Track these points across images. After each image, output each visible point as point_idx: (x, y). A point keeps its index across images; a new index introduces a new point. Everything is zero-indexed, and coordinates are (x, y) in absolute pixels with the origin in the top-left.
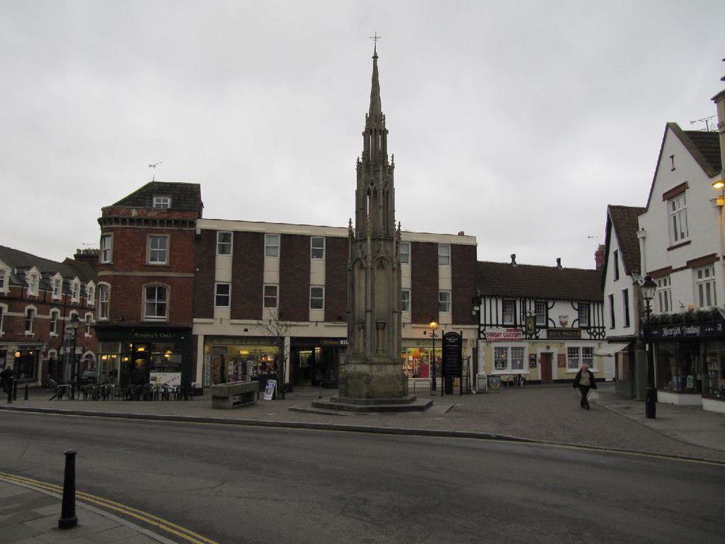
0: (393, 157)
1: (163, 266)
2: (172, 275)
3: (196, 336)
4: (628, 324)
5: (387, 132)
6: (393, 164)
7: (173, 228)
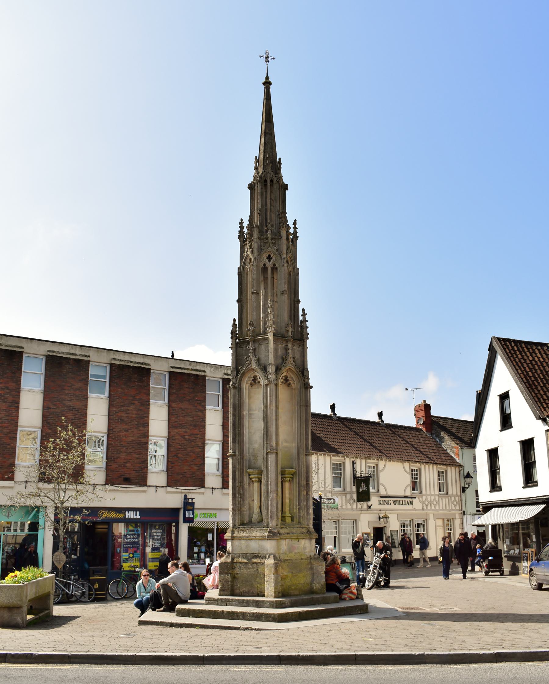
0: (295, 223)
4: (493, 454)
5: (285, 187)
6: (295, 233)
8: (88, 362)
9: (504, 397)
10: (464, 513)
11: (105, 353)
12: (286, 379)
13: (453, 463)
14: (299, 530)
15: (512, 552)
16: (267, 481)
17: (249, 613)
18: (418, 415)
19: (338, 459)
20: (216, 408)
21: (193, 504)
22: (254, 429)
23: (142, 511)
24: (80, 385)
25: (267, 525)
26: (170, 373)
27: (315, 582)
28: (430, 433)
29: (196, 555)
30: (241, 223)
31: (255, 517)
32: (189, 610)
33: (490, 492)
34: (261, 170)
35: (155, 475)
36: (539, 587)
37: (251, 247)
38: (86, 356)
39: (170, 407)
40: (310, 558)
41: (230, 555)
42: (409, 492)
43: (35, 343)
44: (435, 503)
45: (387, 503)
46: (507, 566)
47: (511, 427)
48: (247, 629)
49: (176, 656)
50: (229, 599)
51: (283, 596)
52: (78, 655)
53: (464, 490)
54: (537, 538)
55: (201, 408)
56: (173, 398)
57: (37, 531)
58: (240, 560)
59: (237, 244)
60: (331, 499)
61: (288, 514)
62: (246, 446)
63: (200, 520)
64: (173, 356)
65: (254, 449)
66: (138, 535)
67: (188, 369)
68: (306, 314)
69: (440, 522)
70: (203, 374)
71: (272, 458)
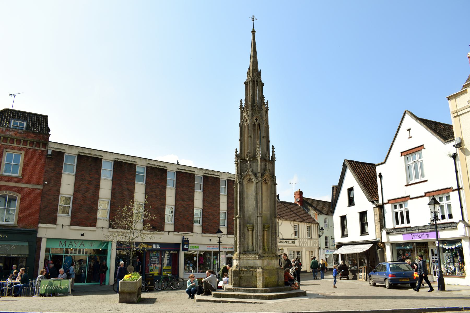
1: (15, 177)
2: (24, 185)
3: (40, 239)
4: (343, 218)
5: (263, 84)
7: (28, 147)
8: (136, 164)
9: (351, 190)
11: (144, 161)
12: (265, 180)
13: (315, 222)
14: (272, 255)
15: (353, 268)
16: (257, 230)
20: (199, 191)
21: (188, 241)
22: (250, 204)
23: (161, 244)
24: (131, 177)
26: (177, 172)
29: (187, 268)
30: (241, 101)
31: (250, 248)
32: (220, 294)
34: (251, 75)
35: (168, 225)
36: (374, 285)
37: (247, 113)
38: (134, 162)
39: (176, 190)
40: (277, 269)
42: (293, 237)
43: (108, 154)
45: (283, 242)
46: (351, 276)
47: (354, 205)
48: (255, 303)
51: (265, 288)
53: (319, 236)
54: (368, 261)
55: (192, 191)
56: (178, 185)
57: (211, 252)
58: (243, 269)
59: (239, 111)
61: (266, 247)
62: (246, 213)
63: (191, 250)
64: (178, 163)
66: (158, 257)
67: (186, 170)
69: (308, 253)
70: (193, 173)
71: (259, 219)
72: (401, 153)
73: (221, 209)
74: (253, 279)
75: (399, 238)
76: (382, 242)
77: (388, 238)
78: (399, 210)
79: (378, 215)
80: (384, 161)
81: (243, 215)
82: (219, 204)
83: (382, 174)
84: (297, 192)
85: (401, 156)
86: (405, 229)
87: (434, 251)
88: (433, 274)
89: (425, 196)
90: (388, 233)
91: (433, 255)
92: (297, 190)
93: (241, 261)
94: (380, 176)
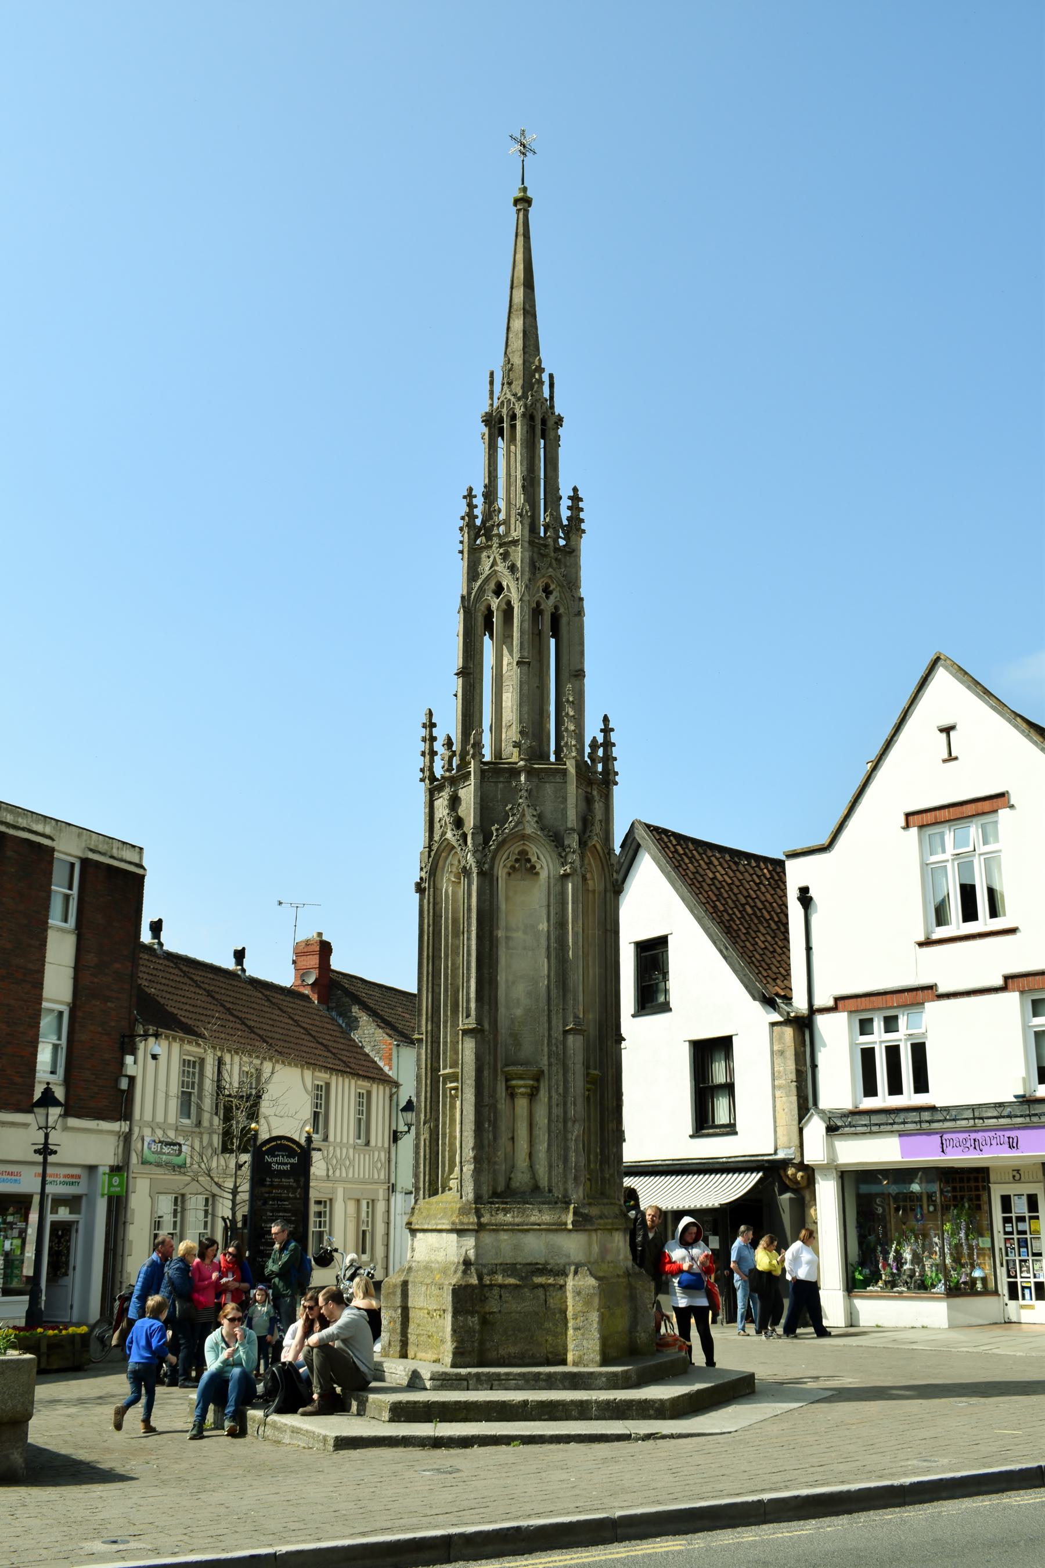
10: (392, 1189)
17: (596, 1402)
18: (300, 964)
19: (194, 1050)
25: (565, 1196)
27: (639, 1328)
28: (325, 1007)
33: (691, 1136)
40: (628, 1274)
41: (473, 1269)
44: (348, 1163)
47: (666, 1008)
49: (849, 1492)
50: (499, 1374)
52: (636, 1516)
58: (499, 1279)
60: (174, 1144)
65: (512, 1021)
68: (612, 730)
69: (352, 1206)
72: (908, 815)
73: (46, 993)
74: (549, 1325)
75: (882, 1151)
76: (802, 1166)
77: (831, 1150)
78: (879, 1039)
79: (790, 1053)
80: (825, 840)
81: (494, 1023)
82: (41, 972)
83: (812, 893)
84: (307, 943)
85: (907, 826)
86: (914, 1116)
87: (1014, 1201)
88: (1006, 1291)
89: (1003, 989)
90: (832, 1130)
91: (1007, 1220)
92: (307, 933)
93: (487, 1238)
94: (805, 898)
